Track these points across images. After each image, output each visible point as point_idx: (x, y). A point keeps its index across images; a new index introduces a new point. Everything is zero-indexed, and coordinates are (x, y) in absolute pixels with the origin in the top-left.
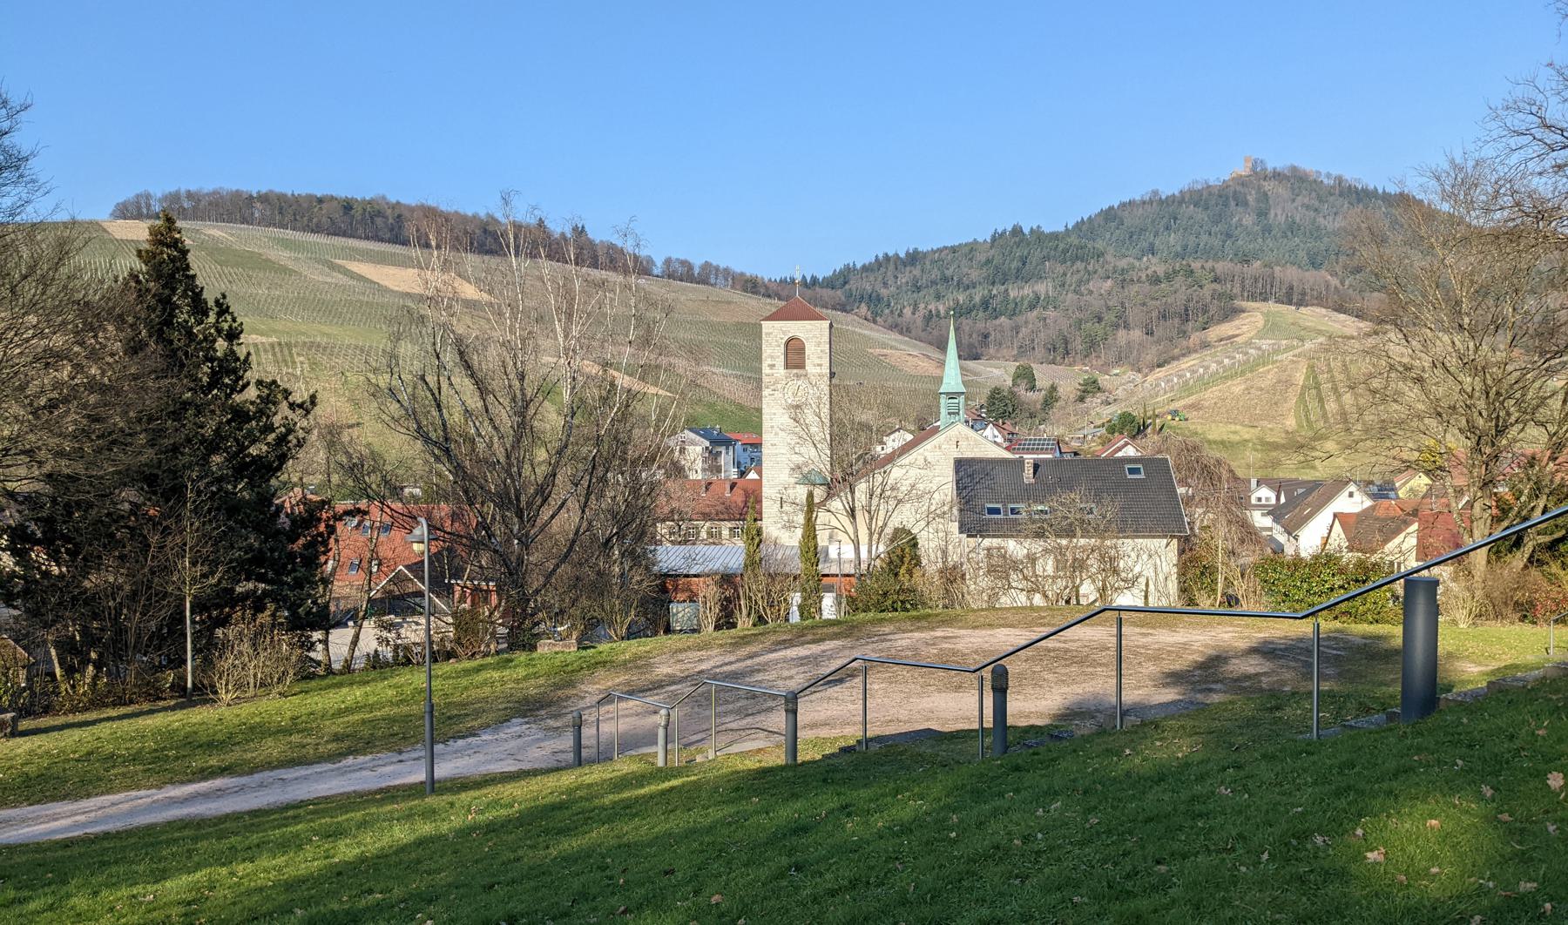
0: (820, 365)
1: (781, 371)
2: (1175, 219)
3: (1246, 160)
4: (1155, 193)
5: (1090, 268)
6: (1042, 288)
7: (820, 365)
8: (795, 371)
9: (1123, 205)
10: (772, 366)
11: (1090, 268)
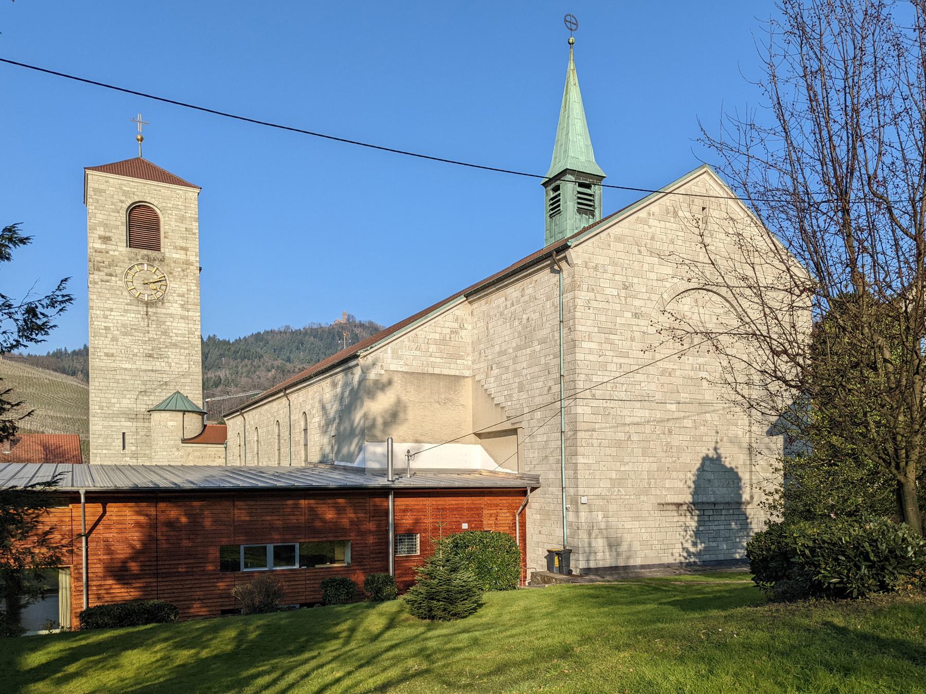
0: (185, 249)
1: (120, 248)
2: (302, 344)
3: (344, 315)
4: (288, 327)
5: (255, 364)
6: (222, 374)
7: (185, 249)
8: (145, 252)
9: (267, 333)
10: (106, 239)
11: (255, 364)
